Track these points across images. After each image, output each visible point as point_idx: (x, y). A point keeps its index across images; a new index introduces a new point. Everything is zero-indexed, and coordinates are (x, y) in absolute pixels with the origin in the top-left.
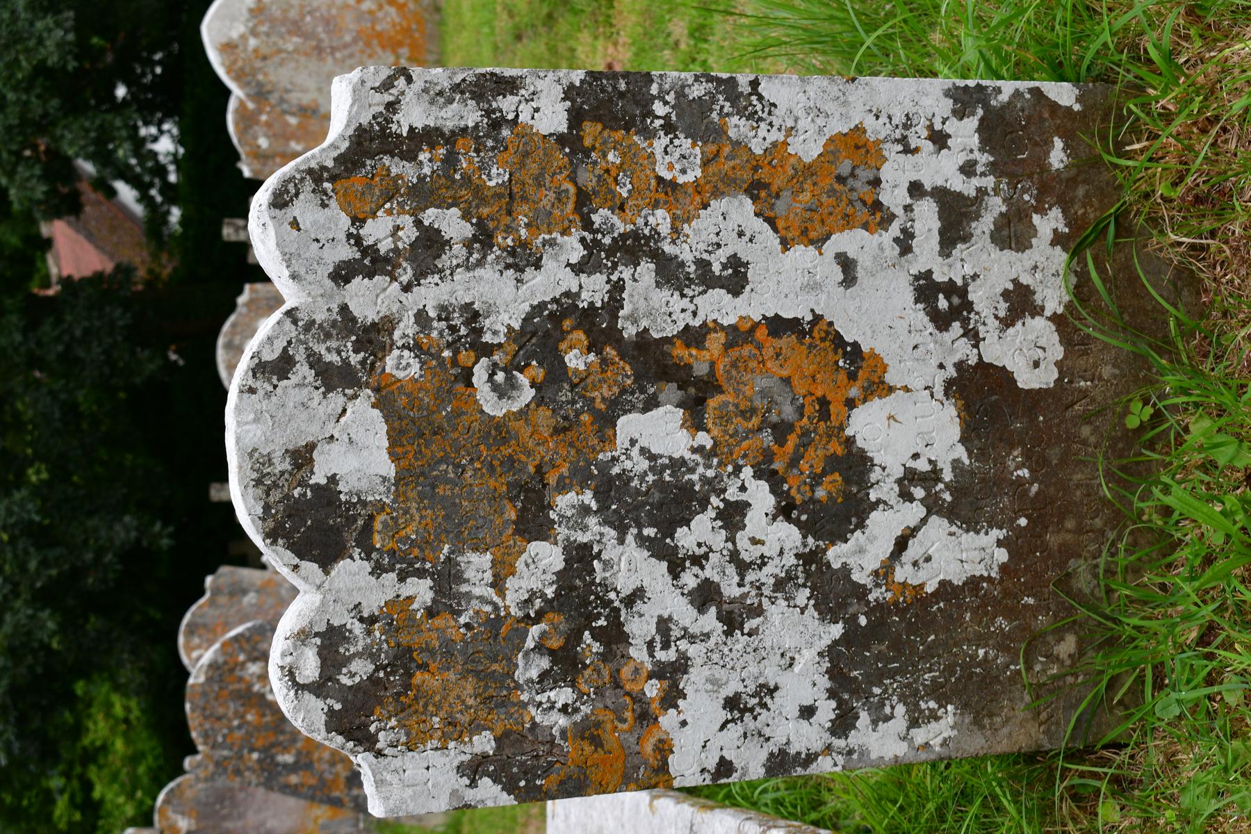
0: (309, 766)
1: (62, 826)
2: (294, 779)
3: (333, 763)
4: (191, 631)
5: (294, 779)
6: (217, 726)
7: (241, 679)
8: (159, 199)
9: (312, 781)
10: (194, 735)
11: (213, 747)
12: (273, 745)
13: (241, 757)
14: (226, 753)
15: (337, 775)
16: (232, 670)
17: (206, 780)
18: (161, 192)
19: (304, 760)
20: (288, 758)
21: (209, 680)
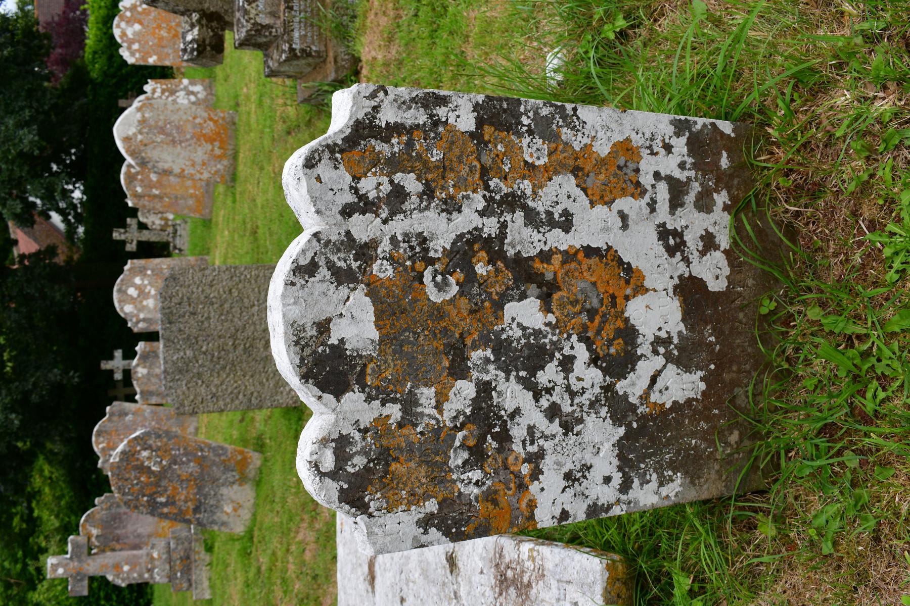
1: (17, 530)
2: (166, 510)
4: (99, 434)
5: (166, 510)
6: (125, 483)
7: (138, 459)
8: (73, 221)
9: (175, 511)
12: (155, 493)
13: (138, 500)
14: (130, 497)
15: (188, 507)
16: (133, 455)
17: (107, 509)
18: (74, 217)
20: (163, 500)
21: (121, 460)
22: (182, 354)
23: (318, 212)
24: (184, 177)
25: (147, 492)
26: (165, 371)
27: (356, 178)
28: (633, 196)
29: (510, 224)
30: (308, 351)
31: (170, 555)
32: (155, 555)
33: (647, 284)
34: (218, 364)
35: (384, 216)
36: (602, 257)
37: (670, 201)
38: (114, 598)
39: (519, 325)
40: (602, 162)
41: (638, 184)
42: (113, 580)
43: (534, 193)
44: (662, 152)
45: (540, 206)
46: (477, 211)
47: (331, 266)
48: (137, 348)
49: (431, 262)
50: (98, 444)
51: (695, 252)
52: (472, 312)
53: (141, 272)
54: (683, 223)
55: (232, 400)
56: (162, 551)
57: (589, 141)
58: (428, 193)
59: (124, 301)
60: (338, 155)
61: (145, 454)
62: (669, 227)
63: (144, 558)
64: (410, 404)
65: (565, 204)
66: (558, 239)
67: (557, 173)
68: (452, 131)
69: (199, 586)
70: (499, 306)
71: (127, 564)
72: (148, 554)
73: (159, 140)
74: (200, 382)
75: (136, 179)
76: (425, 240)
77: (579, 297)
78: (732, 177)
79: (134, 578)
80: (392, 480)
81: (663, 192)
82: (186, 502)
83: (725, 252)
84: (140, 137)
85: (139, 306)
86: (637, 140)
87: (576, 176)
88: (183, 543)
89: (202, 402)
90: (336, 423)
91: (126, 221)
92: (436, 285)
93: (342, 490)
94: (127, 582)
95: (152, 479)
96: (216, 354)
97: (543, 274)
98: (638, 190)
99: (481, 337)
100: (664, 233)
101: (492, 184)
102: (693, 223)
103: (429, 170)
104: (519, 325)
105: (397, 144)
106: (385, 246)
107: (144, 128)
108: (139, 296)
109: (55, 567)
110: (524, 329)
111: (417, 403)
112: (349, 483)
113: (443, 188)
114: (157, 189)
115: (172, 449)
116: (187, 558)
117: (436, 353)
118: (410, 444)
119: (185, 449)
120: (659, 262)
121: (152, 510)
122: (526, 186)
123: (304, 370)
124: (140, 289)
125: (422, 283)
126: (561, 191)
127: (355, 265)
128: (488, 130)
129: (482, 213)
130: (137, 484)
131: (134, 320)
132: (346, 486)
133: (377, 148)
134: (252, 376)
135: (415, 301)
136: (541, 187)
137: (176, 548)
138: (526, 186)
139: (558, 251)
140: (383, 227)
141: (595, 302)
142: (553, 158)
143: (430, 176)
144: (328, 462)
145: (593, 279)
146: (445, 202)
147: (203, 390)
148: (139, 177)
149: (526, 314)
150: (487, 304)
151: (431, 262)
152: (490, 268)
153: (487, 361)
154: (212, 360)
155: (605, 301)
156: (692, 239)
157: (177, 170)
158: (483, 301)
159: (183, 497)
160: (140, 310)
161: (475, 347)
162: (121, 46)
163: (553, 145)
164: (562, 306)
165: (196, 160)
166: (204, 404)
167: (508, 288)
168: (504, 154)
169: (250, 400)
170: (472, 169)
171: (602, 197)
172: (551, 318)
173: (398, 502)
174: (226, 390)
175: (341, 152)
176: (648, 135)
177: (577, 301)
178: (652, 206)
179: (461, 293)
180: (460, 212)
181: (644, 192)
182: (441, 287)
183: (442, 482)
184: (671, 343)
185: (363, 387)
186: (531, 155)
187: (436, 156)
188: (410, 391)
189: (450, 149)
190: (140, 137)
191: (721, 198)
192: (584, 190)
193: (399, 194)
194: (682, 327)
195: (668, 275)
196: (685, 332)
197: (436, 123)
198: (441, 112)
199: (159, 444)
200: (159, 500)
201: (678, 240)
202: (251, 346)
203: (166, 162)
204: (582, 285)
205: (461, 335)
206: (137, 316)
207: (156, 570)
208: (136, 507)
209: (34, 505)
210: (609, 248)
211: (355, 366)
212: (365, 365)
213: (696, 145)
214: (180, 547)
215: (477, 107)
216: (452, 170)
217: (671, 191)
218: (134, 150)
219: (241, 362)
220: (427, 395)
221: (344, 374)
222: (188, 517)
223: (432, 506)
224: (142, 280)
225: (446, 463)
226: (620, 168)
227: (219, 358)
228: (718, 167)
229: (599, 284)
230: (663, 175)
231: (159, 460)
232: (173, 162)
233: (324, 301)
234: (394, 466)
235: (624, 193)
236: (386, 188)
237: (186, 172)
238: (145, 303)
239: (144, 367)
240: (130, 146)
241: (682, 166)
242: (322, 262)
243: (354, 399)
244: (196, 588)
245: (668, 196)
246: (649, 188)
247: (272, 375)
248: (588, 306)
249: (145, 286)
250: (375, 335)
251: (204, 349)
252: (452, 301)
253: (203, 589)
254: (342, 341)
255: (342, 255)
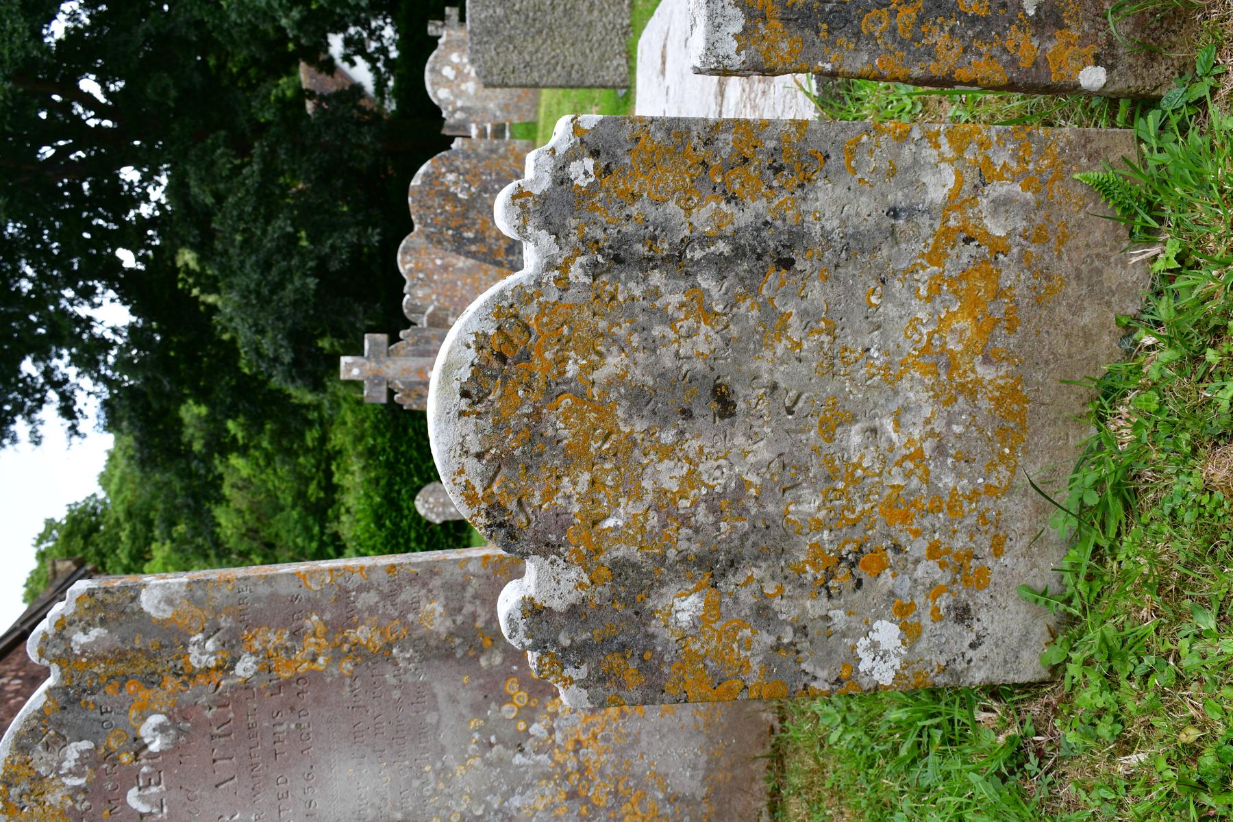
0: (483, 240)
1: (313, 499)
2: (473, 248)
3: (497, 239)
4: (405, 253)
5: (473, 248)
6: (428, 212)
7: (442, 184)
8: (383, 70)
9: (485, 250)
10: (413, 217)
11: (425, 226)
12: (461, 226)
13: (441, 233)
14: (432, 230)
15: (500, 246)
16: (437, 178)
17: (413, 345)
18: (385, 65)
19: (480, 236)
20: (470, 235)
21: (423, 183)
22: (491, 11)
25: (453, 224)
26: (471, 32)
34: (533, 26)
38: (426, 539)
46: (1081, 499)
50: (404, 263)
53: (459, 47)
55: (549, 72)
59: (437, 84)
61: (451, 177)
74: (511, 47)
79: (451, 514)
85: (456, 91)
89: (513, 72)
91: (444, 11)
96: (531, 14)
108: (456, 77)
109: (350, 366)
115: (482, 173)
119: (498, 174)
121: (458, 248)
124: (458, 69)
131: (450, 108)
134: (573, 44)
147: (515, 56)
154: (526, 22)
160: (457, 96)
166: (516, 74)
169: (570, 74)
174: (542, 58)
199: (467, 166)
200: (466, 235)
202: (573, 7)
206: (454, 103)
208: (439, 242)
209: (334, 468)
219: (560, 26)
224: (461, 57)
227: (534, 20)
238: (463, 87)
247: (596, 45)
249: (464, 65)
251: (517, 7)
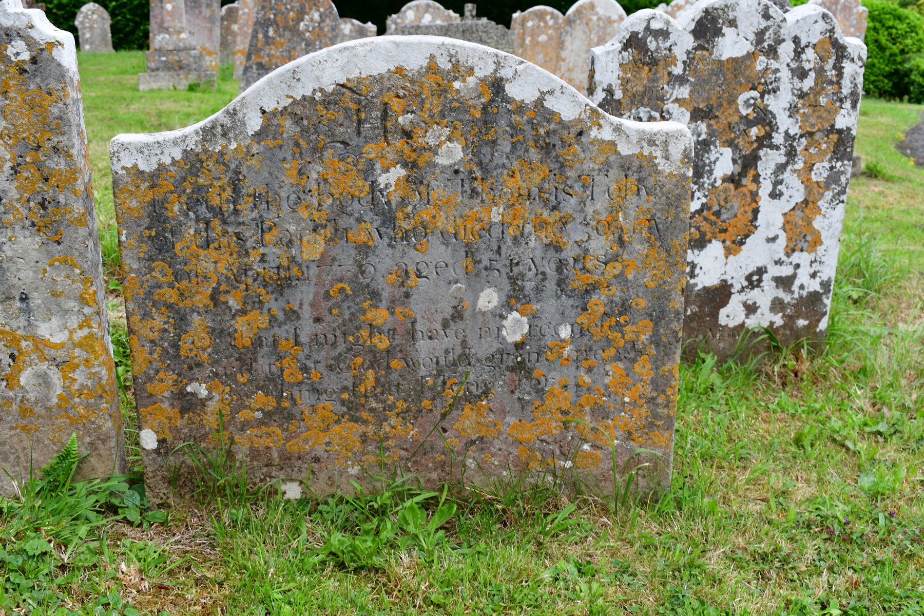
2: (260, 36)
5: (260, 36)
7: (311, 9)
9: (259, 45)
12: (277, 25)
13: (271, 9)
15: (263, 58)
16: (315, 5)
23: (798, 21)
24: (557, 62)
25: (278, 18)
27: (814, 46)
28: (787, 246)
29: (778, 152)
30: (720, 12)
31: (182, 50)
32: (183, 36)
33: (731, 257)
35: (791, 64)
36: (752, 222)
37: (781, 277)
39: (718, 158)
40: (809, 223)
41: (793, 251)
42: (82, 13)
43: (795, 171)
44: (812, 271)
45: (787, 176)
47: (767, 28)
48: (370, 24)
49: (762, 97)
51: (746, 298)
52: (730, 124)
54: (766, 288)
56: (187, 42)
57: (823, 212)
58: (802, 95)
59: (418, 10)
60: (828, 35)
61: (316, 16)
62: (765, 276)
63: (179, 25)
64: (682, 80)
65: (787, 193)
66: (766, 187)
67: (806, 187)
68: (836, 112)
69: (152, 79)
70: (731, 144)
71: (173, 7)
72: (182, 28)
73: (592, 36)
75: (540, 21)
76: (775, 92)
77: (729, 204)
78: (791, 329)
79: (84, 34)
80: (639, 67)
81: (786, 271)
82: (268, 55)
83: (743, 324)
84: (594, 18)
86: (820, 249)
87: (802, 202)
88: (196, 63)
90: (677, 30)
92: (748, 100)
93: (638, 33)
94: (79, 27)
95: (291, 23)
97: (746, 176)
98: (790, 251)
99: (714, 131)
100: (761, 271)
101: (803, 140)
102: (764, 296)
103: (815, 95)
104: (718, 158)
105: (831, 74)
106: (774, 65)
107: (604, 23)
110: (715, 162)
111: (681, 85)
112: (641, 39)
113: (804, 105)
114: (531, 41)
115: (321, 42)
116: (180, 67)
117: (708, 99)
118: (657, 80)
120: (744, 267)
121: (260, 23)
122: (800, 165)
123: (711, 10)
125: (751, 89)
126: (794, 191)
127: (765, 44)
128: (834, 137)
129: (787, 133)
130: (286, 8)
132: (640, 36)
133: (830, 61)
135: (741, 84)
136: (798, 176)
137: (190, 56)
138: (800, 165)
139: (759, 187)
140: (785, 64)
141: (724, 217)
142: (815, 185)
143: (811, 96)
144: (655, 25)
145: (738, 215)
146: (795, 107)
148: (542, 24)
149: (723, 163)
150: (733, 135)
151: (762, 97)
152: (754, 138)
153: (699, 135)
155: (724, 224)
156: (754, 295)
157: (564, 54)
158: (735, 132)
159: (273, 52)
161: (709, 126)
162: (668, 4)
163: (822, 185)
164: (726, 190)
165: (575, 73)
167: (740, 150)
168: (820, 149)
170: (813, 125)
171: (788, 222)
172: (719, 182)
173: (625, 72)
175: (830, 37)
176: (823, 259)
177: (726, 202)
178: (779, 262)
179: (741, 117)
180: (790, 116)
181: (788, 255)
182: (746, 102)
183: (632, 102)
184: (691, 277)
185: (695, 49)
186: (818, 169)
187: (823, 100)
188: (688, 81)
189: (826, 110)
190: (594, 18)
191: (778, 320)
192: (793, 209)
193: (802, 74)
194: (700, 287)
195: (734, 275)
196: (696, 289)
197: (841, 100)
198: (848, 104)
199: (326, 29)
201: (755, 283)
203: (572, 43)
204: (736, 205)
205: (717, 117)
207: (167, 36)
208: (263, 8)
210: (756, 227)
211: (708, 43)
212: (708, 50)
213: (814, 299)
214: (191, 60)
215: (849, 129)
216: (814, 111)
217: (787, 277)
218: (582, 13)
220: (684, 92)
221: (705, 37)
222: (253, 58)
223: (618, 95)
225: (642, 105)
226: (805, 236)
228: (798, 318)
229: (735, 219)
230: (798, 271)
231: (310, 29)
232: (572, 51)
233: (748, 24)
234: (646, 68)
235: (789, 239)
236: (807, 66)
237: (562, 63)
239: (351, 31)
240: (585, 9)
241: (802, 287)
242: (770, 23)
243: (689, 42)
244: (150, 76)
245: (784, 275)
246: (790, 260)
248: (723, 211)
250: (724, 58)
252: (738, 111)
253: (149, 83)
254: (724, 35)
255: (772, 36)
